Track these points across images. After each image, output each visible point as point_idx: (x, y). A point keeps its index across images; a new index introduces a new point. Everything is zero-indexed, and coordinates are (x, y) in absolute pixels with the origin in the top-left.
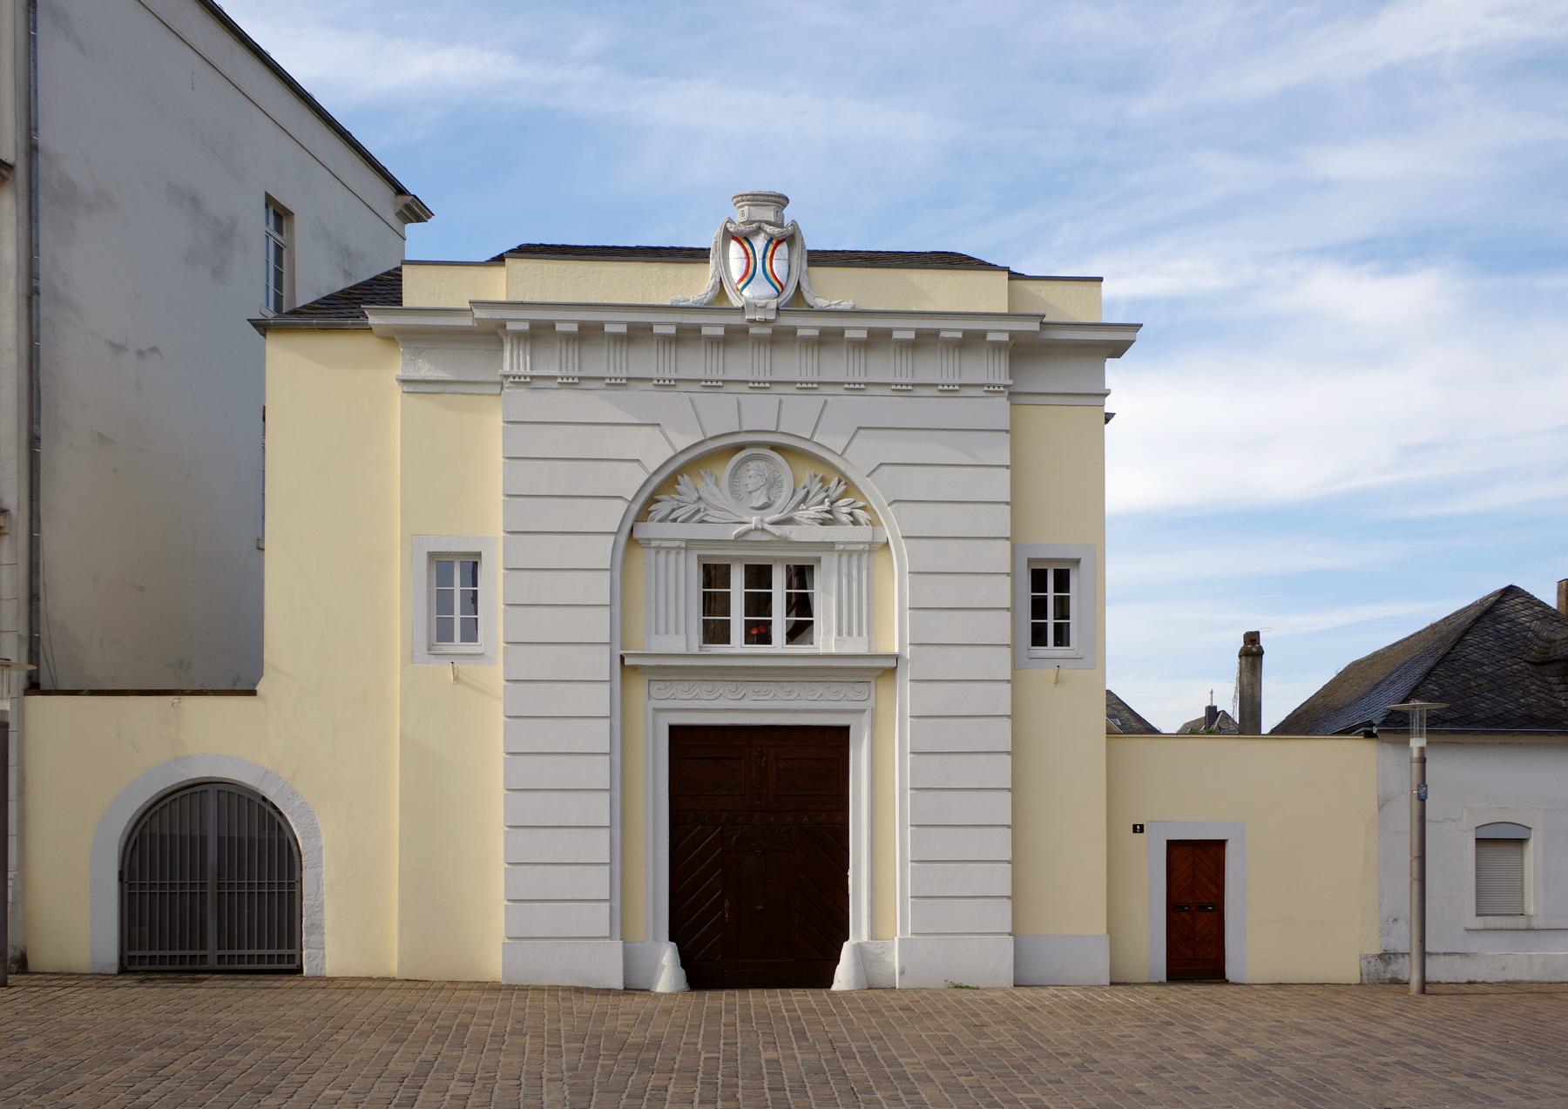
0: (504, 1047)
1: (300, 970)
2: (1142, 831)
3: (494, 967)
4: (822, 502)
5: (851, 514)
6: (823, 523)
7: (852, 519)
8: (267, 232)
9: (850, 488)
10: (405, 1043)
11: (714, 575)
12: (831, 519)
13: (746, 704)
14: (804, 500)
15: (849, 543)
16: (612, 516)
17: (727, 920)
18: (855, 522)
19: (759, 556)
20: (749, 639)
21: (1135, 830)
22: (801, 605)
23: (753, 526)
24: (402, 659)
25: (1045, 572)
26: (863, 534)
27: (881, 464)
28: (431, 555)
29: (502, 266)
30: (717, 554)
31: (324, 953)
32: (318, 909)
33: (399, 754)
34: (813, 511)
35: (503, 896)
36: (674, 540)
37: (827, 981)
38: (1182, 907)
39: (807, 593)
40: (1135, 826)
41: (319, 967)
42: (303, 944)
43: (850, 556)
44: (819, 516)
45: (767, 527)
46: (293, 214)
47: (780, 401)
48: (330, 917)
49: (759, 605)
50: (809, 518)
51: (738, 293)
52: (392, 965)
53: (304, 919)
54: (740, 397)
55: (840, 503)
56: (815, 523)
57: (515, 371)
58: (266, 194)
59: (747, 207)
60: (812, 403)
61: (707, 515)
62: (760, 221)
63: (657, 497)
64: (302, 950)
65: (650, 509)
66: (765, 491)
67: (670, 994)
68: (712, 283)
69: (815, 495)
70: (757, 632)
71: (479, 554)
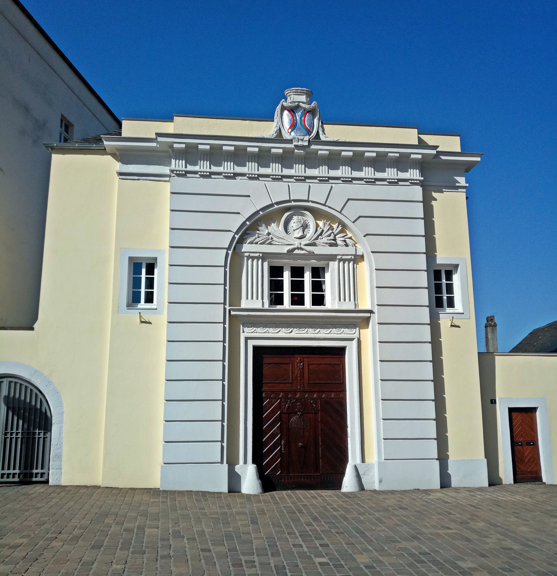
0: (172, 553)
1: (47, 482)
3: (156, 482)
4: (330, 235)
5: (345, 241)
6: (331, 245)
7: (345, 243)
8: (61, 131)
9: (344, 227)
10: (102, 549)
11: (276, 272)
12: (334, 244)
13: (293, 335)
14: (321, 234)
15: (344, 255)
16: (225, 240)
17: (283, 452)
18: (347, 245)
19: (298, 263)
20: (293, 303)
22: (317, 286)
23: (296, 246)
24: (113, 311)
26: (350, 250)
27: (360, 217)
28: (130, 259)
29: (171, 122)
30: (277, 263)
31: (61, 472)
32: (60, 447)
33: (116, 213)
34: (324, 239)
35: (162, 440)
36: (256, 253)
37: (338, 485)
38: (518, 443)
39: (320, 281)
41: (58, 480)
42: (50, 467)
43: (344, 263)
44: (329, 242)
45: (302, 246)
46: (73, 126)
47: (310, 186)
48: (65, 451)
49: (297, 286)
50: (324, 243)
51: (289, 134)
52: (99, 480)
53: (51, 452)
54: (290, 184)
55: (339, 235)
56: (326, 245)
57: (177, 168)
58: (62, 114)
59: (292, 95)
60: (326, 187)
61: (273, 241)
62: (299, 102)
63: (248, 232)
64: (49, 470)
65: (244, 237)
66: (301, 230)
67: (254, 495)
68: (275, 130)
69: (325, 233)
70: (298, 300)
71: (156, 259)
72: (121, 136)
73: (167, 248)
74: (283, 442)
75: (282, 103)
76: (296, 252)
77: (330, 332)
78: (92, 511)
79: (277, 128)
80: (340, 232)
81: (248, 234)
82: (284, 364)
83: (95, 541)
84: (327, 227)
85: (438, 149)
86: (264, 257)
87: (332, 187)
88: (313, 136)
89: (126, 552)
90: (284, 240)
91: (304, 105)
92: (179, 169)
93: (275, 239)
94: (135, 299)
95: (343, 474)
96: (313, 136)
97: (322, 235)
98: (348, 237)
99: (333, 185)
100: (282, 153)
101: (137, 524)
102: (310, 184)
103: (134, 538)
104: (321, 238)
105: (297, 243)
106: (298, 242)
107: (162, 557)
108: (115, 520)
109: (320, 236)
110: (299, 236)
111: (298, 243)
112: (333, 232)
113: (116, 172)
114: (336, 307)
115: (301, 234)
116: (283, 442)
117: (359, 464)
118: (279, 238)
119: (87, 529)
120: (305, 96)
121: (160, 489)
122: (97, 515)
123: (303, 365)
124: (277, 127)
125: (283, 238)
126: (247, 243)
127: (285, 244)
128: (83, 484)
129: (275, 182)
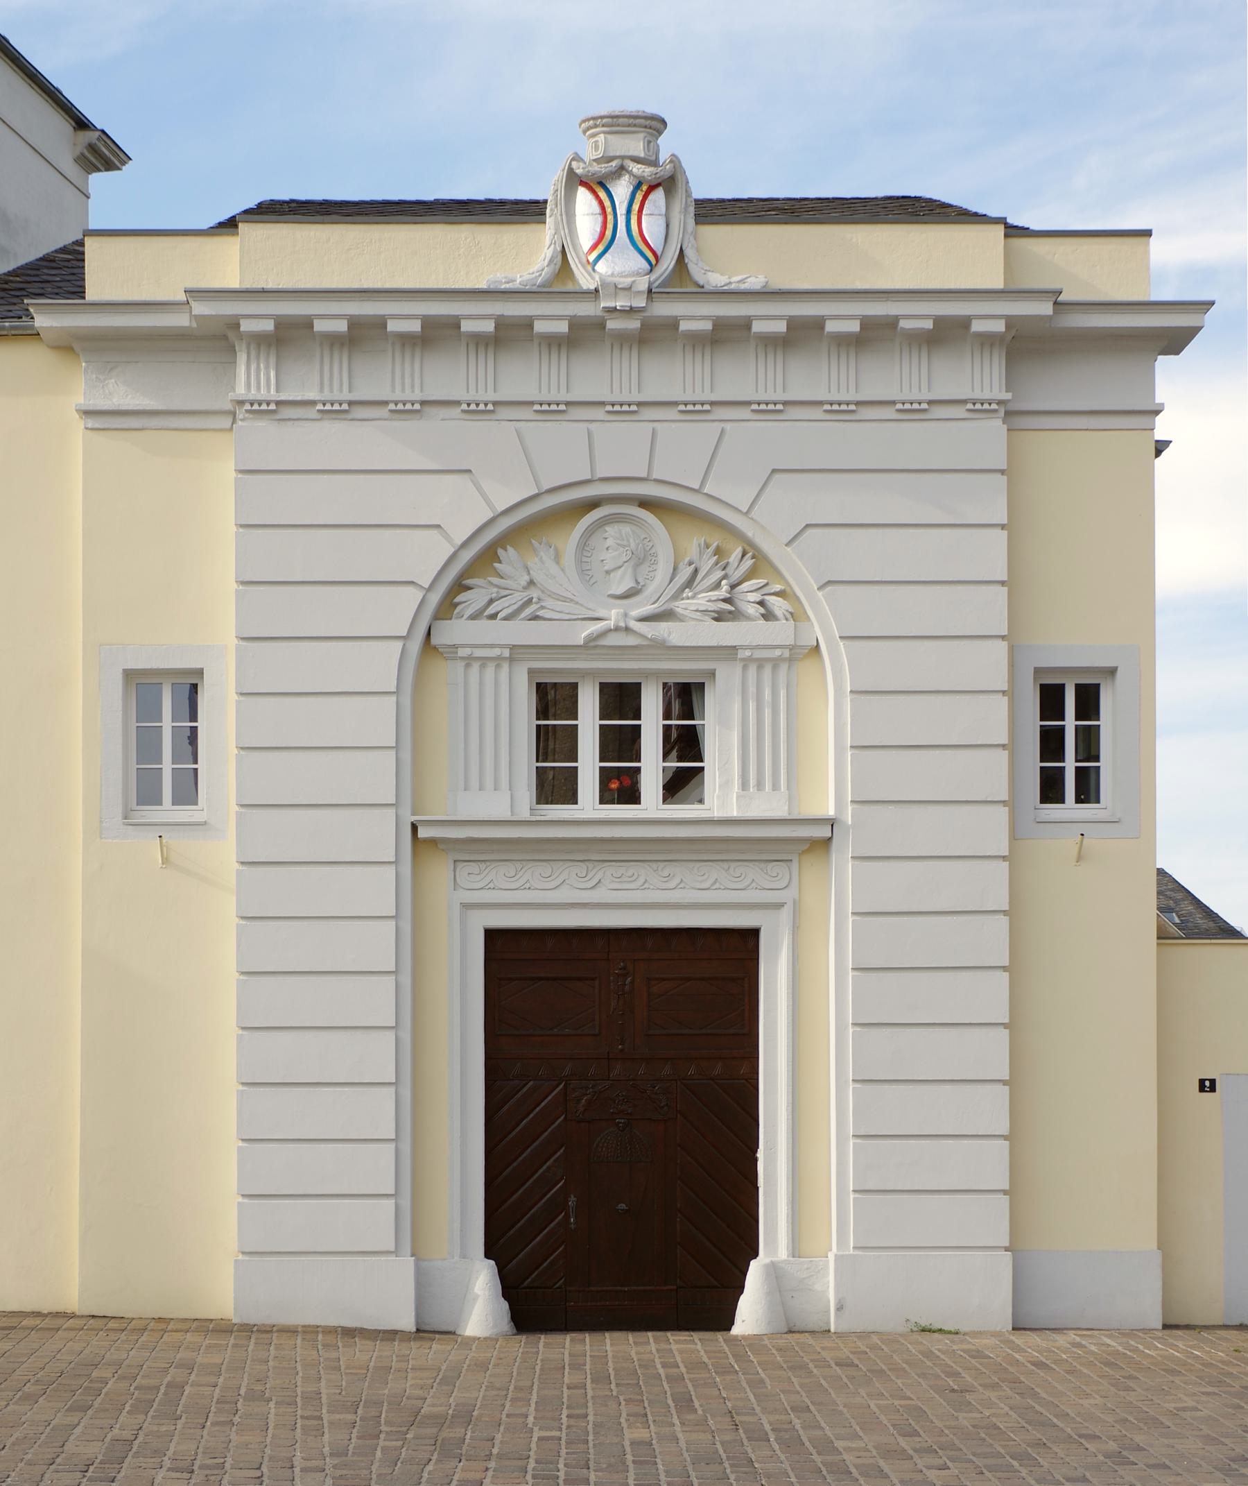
0: (237, 1419)
2: (1213, 1088)
4: (717, 586)
6: (719, 617)
7: (762, 610)
9: (760, 563)
10: (90, 1412)
12: (730, 612)
15: (758, 647)
18: (768, 616)
19: (621, 669)
21: (1202, 1088)
23: (612, 624)
25: (1061, 689)
26: (780, 633)
27: (808, 526)
34: (703, 600)
36: (492, 646)
37: (724, 1320)
40: (1202, 1082)
44: (712, 606)
47: (654, 432)
50: (697, 611)
51: (589, 268)
54: (593, 426)
55: (745, 586)
59: (602, 135)
61: (543, 608)
62: (623, 158)
66: (630, 571)
72: (84, 298)
73: (233, 642)
74: (572, 1200)
75: (570, 164)
76: (612, 640)
77: (712, 885)
78: (58, 1358)
79: (555, 248)
80: (750, 575)
81: (469, 588)
82: (579, 979)
83: (74, 1401)
84: (709, 560)
85: (1061, 298)
86: (516, 653)
87: (723, 431)
88: (667, 268)
89: (142, 1417)
90: (577, 603)
91: (639, 166)
92: (259, 398)
93: (549, 603)
94: (148, 793)
95: (738, 1288)
96: (667, 268)
97: (694, 585)
98: (772, 591)
99: (728, 426)
100: (784, 335)
101: (169, 1378)
102: (655, 424)
103: (157, 1400)
104: (690, 594)
105: (613, 615)
106: (617, 610)
107: (214, 1424)
108: (116, 1372)
109: (687, 590)
110: (620, 590)
111: (618, 613)
112: (725, 577)
113: (76, 410)
114: (734, 812)
115: (626, 585)
116: (572, 1200)
117: (785, 1260)
118: (561, 598)
119: (54, 1385)
120: (642, 135)
121: (233, 1321)
122: (72, 1365)
123: (632, 982)
124: (553, 246)
125: (572, 597)
126: (465, 617)
127: (580, 617)
128: (29, 1309)
129: (549, 424)
